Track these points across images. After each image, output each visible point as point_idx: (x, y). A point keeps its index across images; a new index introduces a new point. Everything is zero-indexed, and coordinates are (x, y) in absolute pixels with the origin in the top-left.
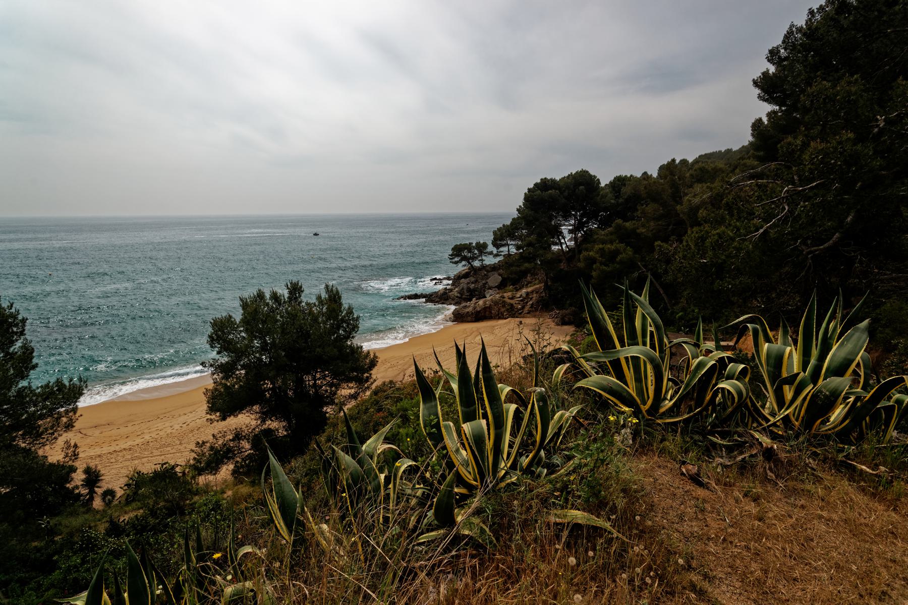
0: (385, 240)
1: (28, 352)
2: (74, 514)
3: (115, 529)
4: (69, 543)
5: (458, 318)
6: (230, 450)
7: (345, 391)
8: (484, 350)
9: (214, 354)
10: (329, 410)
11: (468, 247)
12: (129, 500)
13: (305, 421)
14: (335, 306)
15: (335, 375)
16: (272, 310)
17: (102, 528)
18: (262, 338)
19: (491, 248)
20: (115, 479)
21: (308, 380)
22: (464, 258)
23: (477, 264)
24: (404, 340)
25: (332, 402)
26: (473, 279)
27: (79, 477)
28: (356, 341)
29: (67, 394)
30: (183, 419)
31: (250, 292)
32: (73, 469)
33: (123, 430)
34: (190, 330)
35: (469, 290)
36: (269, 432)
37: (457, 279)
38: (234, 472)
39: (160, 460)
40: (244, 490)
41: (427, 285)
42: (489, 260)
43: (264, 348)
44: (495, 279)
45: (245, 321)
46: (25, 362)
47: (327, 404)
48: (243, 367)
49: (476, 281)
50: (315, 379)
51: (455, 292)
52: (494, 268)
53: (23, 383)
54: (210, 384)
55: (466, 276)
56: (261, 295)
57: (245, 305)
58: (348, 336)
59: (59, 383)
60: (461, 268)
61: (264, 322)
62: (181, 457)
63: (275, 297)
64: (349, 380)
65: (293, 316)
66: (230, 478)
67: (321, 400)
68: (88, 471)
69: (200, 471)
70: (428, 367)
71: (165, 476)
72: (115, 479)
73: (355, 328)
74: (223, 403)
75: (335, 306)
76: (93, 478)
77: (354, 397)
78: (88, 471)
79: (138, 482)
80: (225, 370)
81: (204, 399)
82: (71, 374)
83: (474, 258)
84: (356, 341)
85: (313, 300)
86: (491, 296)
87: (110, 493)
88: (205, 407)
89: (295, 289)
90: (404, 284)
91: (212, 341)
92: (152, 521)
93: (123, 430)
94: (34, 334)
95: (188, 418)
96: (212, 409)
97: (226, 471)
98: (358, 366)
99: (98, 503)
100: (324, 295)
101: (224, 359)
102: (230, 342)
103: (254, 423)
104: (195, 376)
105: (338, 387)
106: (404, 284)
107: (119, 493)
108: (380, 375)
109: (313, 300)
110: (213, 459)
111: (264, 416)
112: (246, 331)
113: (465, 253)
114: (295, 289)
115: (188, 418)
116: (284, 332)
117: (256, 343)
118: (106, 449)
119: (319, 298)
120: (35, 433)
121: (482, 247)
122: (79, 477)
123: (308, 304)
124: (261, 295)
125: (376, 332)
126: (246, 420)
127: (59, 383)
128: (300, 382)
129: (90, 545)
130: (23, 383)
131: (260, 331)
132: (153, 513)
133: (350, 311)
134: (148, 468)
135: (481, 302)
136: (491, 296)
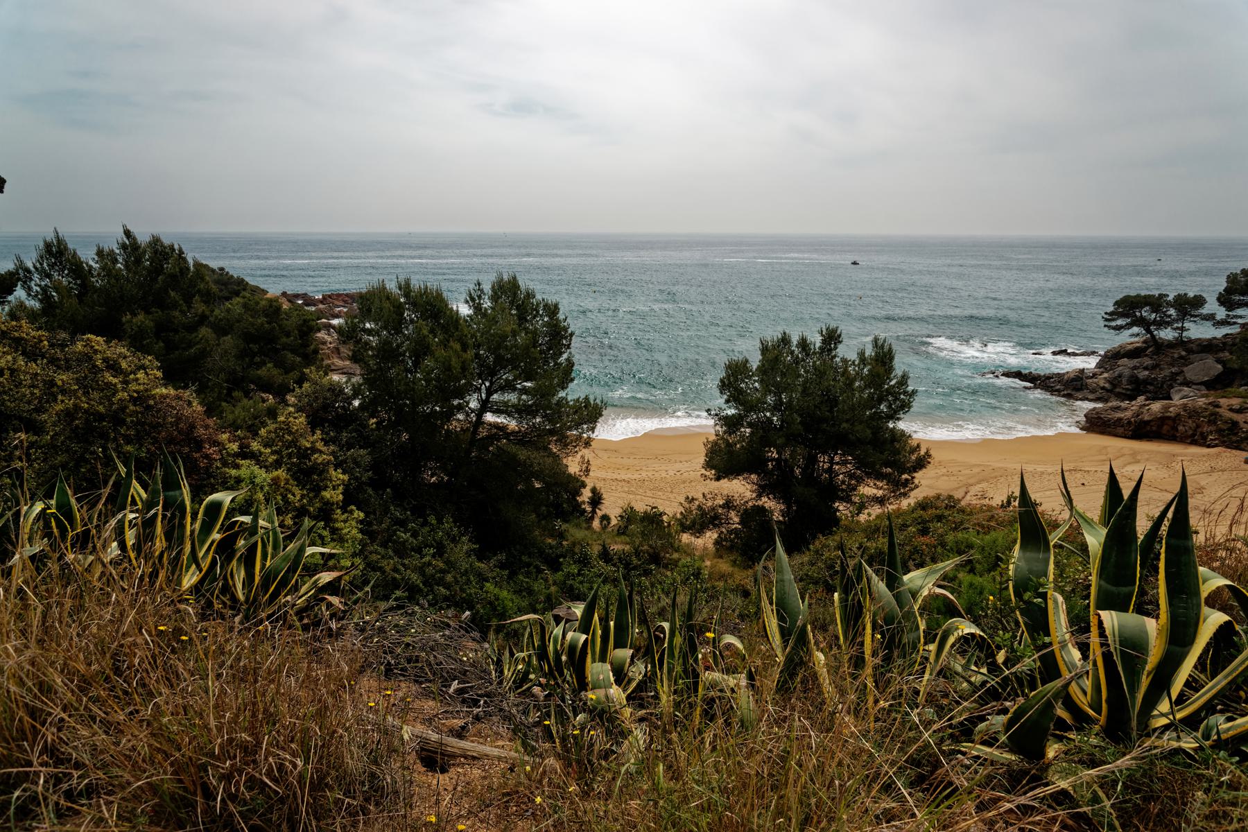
0: (981, 278)
1: (570, 364)
2: (578, 526)
3: (605, 555)
4: (571, 550)
5: (1095, 424)
6: (716, 517)
7: (868, 490)
8: (1112, 476)
9: (720, 401)
10: (842, 508)
11: (1156, 303)
12: (622, 531)
13: (811, 515)
14: (882, 370)
15: (861, 463)
16: (797, 361)
17: (596, 550)
18: (778, 394)
19: (1212, 306)
20: (612, 508)
21: (823, 461)
22: (1141, 322)
23: (1167, 334)
24: (985, 438)
25: (847, 499)
26: (1147, 362)
27: (586, 494)
28: (903, 425)
29: (591, 413)
30: (678, 466)
31: (772, 334)
32: (584, 485)
33: (626, 461)
34: (696, 370)
35: (1134, 380)
36: (761, 510)
37: (1111, 358)
38: (717, 543)
39: (651, 502)
40: (724, 566)
41: (1048, 362)
42: (1198, 331)
43: (776, 408)
44: (1210, 367)
45: (762, 370)
46: (566, 375)
47: (842, 499)
48: (750, 425)
49: (1154, 367)
50: (831, 462)
51: (1102, 380)
52: (1208, 347)
53: (562, 394)
54: (713, 438)
55: (1134, 353)
56: (785, 340)
57: (765, 350)
58: (893, 416)
59: (587, 398)
60: (1130, 337)
61: (783, 375)
62: (671, 508)
63: (804, 344)
64: (880, 476)
65: (820, 373)
66: (710, 546)
67: (832, 492)
68: (594, 490)
69: (684, 528)
70: (1049, 503)
71: (653, 519)
72: (612, 508)
73: (905, 406)
74: (723, 461)
75: (882, 370)
76: (596, 500)
77: (881, 501)
78: (594, 490)
79: (629, 516)
80: (731, 424)
81: (703, 451)
82: (596, 393)
83: (1161, 324)
84: (903, 425)
85: (853, 356)
86: (1179, 399)
87: (605, 518)
88: (702, 459)
89: (832, 338)
90: (1004, 353)
91: (724, 386)
92: (635, 561)
93: (626, 461)
94: (577, 351)
95: (683, 467)
96: (709, 465)
97: (711, 536)
98: (896, 460)
99: (596, 524)
100: (869, 352)
101: (731, 412)
102: (741, 391)
103: (748, 495)
104: (698, 423)
105: (860, 480)
106: (1004, 353)
107: (614, 522)
108: (927, 484)
109: (853, 356)
110: (701, 520)
111: (762, 491)
112: (761, 381)
113: (1145, 313)
114: (832, 338)
115: (683, 467)
116: (805, 391)
117: (770, 399)
118: (610, 475)
119: (861, 354)
120: (564, 442)
121: (1188, 306)
122: (586, 494)
123: (844, 361)
124: (785, 340)
125: (931, 416)
126: (740, 488)
127: (587, 398)
128: (812, 460)
129: (584, 561)
130: (562, 394)
131: (777, 385)
132: (637, 553)
133: (904, 380)
134: (640, 507)
135: (1156, 406)
136: (1179, 399)
